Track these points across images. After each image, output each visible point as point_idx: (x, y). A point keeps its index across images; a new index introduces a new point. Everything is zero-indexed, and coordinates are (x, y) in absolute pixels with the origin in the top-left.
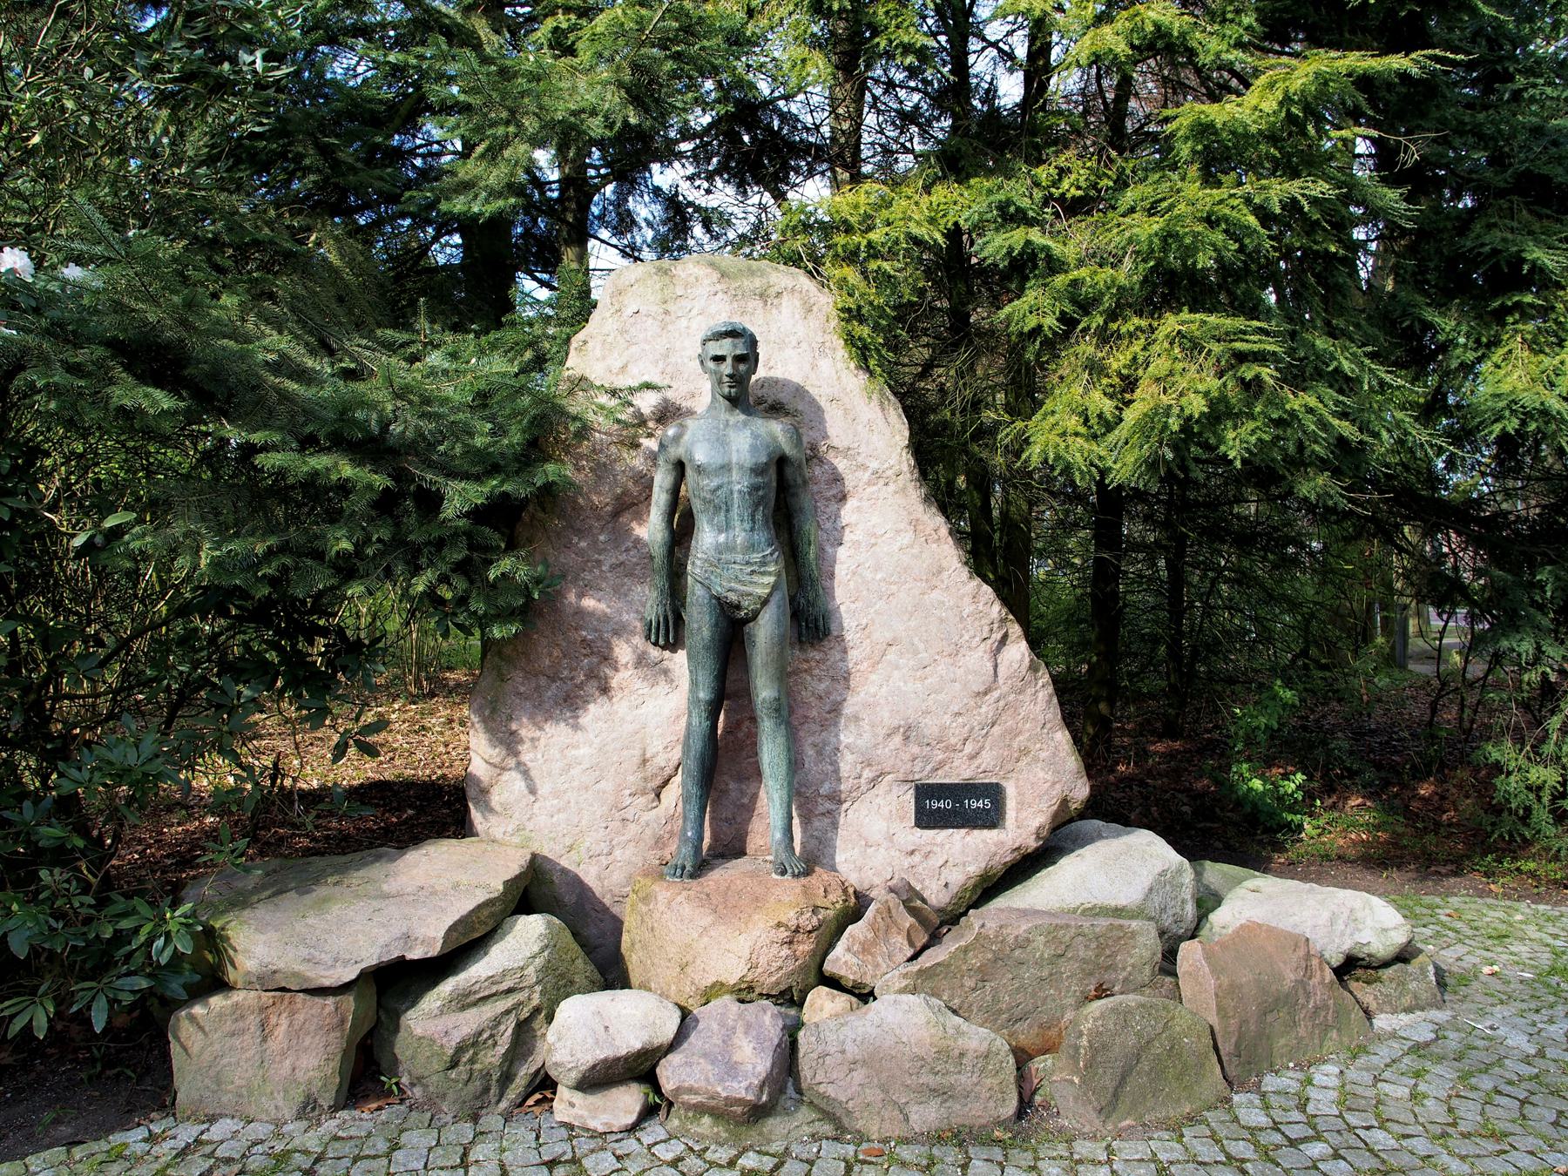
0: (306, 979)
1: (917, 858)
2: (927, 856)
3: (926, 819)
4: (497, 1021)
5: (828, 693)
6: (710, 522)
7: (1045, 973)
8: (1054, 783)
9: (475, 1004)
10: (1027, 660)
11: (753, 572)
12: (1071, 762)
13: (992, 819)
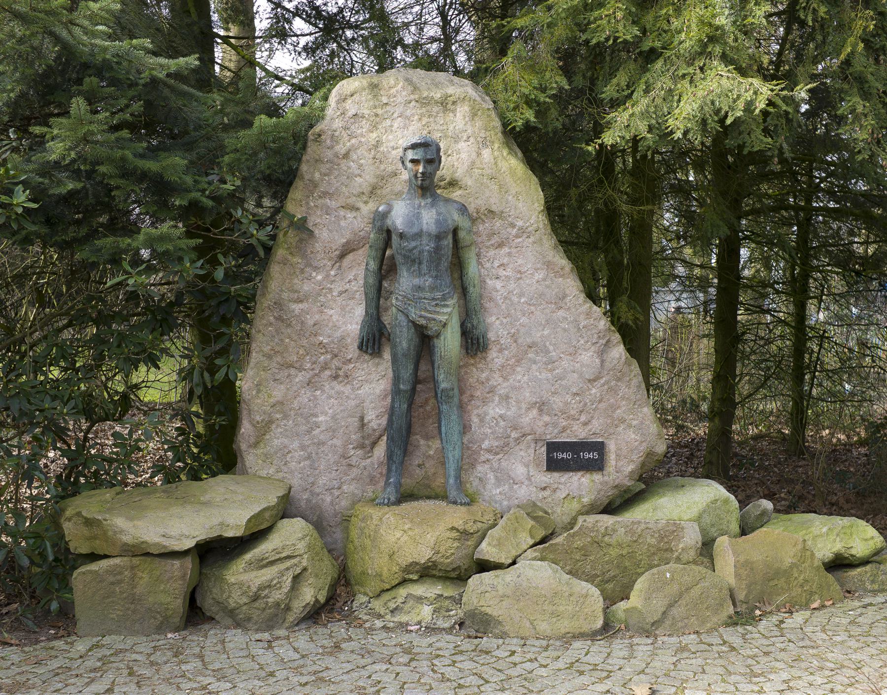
0: (165, 547)
1: (547, 493)
2: (555, 491)
3: (553, 465)
4: (282, 574)
5: (488, 380)
6: (408, 270)
7: (624, 552)
8: (642, 442)
9: (265, 566)
10: (624, 358)
11: (437, 305)
13: (597, 466)
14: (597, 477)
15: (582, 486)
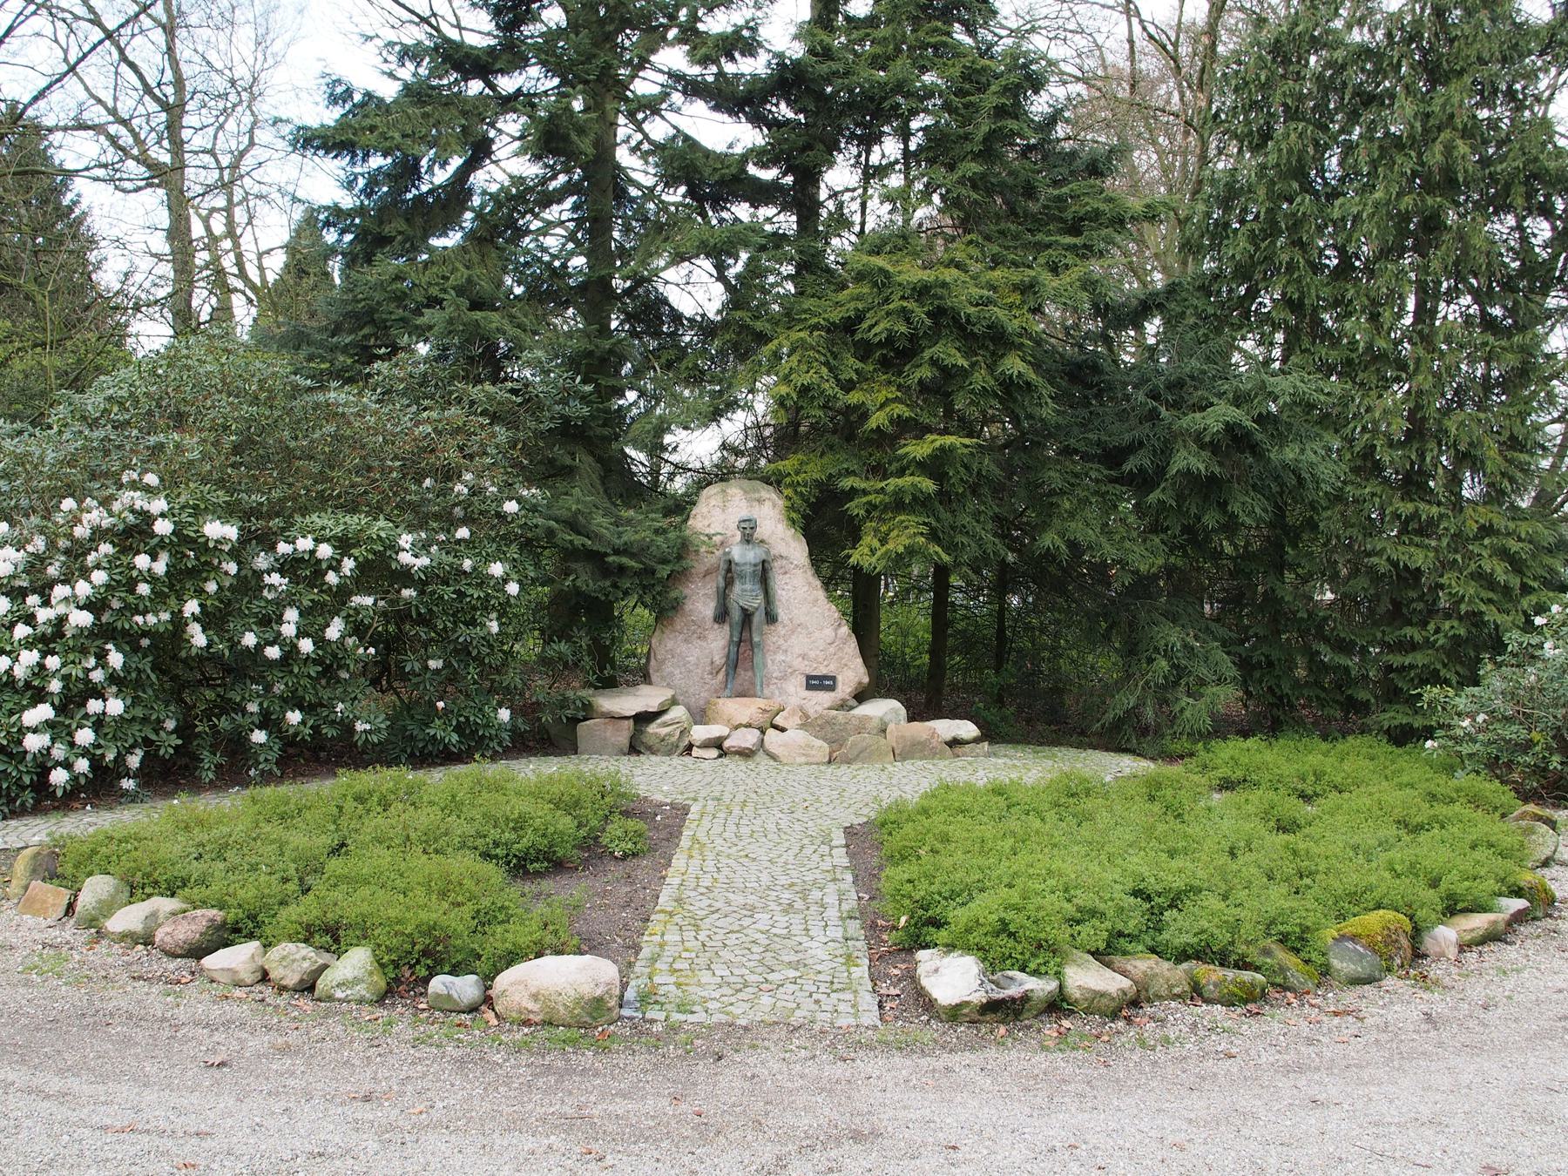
3: (809, 687)
12: (862, 669)
14: (832, 694)
15: (823, 699)
